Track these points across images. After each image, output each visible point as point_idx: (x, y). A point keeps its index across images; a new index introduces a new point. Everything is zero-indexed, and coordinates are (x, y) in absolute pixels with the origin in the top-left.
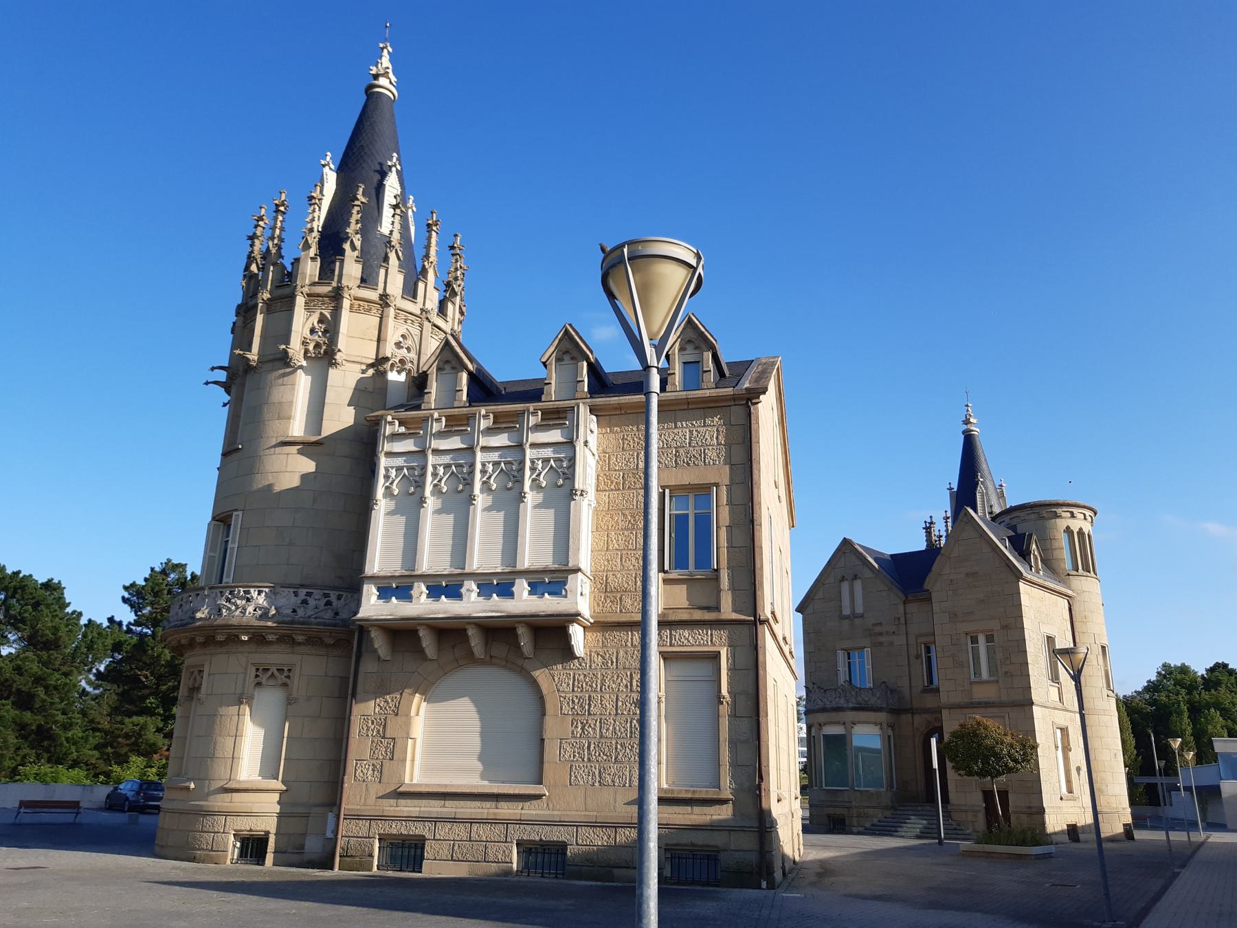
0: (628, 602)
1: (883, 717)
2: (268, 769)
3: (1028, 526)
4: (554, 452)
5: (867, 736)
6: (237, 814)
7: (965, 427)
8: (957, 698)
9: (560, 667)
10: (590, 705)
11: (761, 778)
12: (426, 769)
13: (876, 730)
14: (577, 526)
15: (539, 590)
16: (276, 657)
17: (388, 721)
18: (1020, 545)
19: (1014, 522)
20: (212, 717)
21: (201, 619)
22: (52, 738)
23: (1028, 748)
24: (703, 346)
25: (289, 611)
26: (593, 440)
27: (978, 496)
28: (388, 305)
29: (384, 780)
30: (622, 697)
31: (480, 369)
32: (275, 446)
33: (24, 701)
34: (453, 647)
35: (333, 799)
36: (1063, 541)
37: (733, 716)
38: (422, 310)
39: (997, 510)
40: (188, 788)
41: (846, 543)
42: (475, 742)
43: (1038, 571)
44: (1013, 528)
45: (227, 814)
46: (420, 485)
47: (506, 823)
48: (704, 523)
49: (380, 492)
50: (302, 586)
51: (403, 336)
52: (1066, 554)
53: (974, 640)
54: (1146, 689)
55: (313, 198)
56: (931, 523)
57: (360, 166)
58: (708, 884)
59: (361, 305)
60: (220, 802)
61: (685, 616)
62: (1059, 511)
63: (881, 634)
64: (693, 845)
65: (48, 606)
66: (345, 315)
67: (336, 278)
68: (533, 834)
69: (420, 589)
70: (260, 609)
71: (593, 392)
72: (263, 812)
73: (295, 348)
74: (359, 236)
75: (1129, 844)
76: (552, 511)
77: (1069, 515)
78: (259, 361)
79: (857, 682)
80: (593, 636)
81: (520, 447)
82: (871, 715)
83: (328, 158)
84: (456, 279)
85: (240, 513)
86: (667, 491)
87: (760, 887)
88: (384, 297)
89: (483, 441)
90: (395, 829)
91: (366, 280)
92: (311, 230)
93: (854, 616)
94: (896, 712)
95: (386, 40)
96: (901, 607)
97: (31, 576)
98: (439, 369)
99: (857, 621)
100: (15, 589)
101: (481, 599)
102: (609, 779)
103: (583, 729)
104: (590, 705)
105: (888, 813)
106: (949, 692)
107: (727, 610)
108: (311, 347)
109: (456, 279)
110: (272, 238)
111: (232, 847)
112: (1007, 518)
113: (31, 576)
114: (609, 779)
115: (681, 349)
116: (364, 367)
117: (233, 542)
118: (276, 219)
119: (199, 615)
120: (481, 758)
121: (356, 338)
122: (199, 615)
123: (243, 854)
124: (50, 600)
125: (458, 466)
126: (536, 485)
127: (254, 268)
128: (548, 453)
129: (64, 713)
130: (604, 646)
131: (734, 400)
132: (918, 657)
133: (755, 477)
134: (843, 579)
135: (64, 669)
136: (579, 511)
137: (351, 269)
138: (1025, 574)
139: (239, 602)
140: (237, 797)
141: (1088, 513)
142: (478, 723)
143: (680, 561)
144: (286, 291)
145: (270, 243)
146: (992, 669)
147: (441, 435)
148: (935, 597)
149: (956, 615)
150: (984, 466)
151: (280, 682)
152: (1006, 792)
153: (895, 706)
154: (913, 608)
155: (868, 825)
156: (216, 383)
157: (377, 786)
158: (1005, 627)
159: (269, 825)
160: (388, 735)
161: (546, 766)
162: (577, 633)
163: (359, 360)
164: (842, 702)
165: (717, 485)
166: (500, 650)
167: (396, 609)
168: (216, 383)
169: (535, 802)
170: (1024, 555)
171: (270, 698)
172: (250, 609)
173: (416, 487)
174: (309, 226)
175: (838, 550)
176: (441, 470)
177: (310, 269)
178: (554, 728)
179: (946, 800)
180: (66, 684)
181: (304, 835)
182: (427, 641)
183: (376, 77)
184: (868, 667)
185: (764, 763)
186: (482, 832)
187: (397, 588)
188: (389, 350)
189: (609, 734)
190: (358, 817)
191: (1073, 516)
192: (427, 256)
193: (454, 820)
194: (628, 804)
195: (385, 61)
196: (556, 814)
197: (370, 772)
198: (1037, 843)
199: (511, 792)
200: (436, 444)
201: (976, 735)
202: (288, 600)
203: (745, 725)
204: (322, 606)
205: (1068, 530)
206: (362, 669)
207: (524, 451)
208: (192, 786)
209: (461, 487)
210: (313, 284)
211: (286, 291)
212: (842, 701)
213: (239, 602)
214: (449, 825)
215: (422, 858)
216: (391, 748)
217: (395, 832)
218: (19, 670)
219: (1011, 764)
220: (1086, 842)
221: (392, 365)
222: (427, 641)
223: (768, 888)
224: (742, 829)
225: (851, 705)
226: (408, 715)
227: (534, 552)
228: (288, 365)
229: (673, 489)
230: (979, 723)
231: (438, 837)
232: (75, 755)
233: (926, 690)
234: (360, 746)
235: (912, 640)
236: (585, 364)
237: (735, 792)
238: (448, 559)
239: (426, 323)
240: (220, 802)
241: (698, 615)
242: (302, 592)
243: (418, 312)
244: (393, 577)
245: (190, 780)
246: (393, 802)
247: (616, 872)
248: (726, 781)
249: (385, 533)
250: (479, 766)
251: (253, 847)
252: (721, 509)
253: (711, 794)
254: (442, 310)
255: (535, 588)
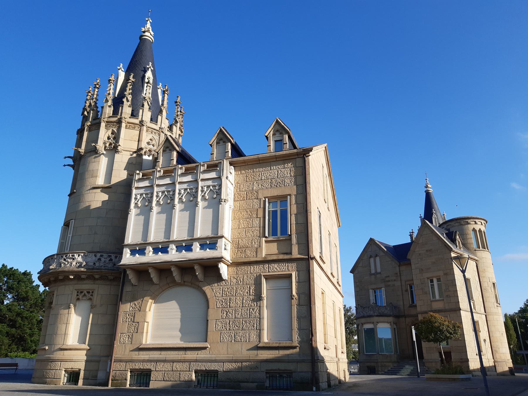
0: (248, 252)
1: (391, 319)
2: (82, 340)
3: (455, 228)
4: (213, 182)
5: (384, 331)
6: (66, 361)
7: (426, 189)
8: (424, 309)
9: (216, 285)
10: (230, 303)
11: (312, 335)
12: (154, 337)
13: (388, 326)
14: (227, 218)
15: (205, 247)
16: (86, 286)
17: (136, 314)
18: (451, 237)
19: (449, 227)
20: (57, 315)
21: (52, 269)
22: (25, 341)
23: (458, 327)
24: (284, 132)
25: (92, 264)
26: (232, 178)
27: (433, 219)
28: (143, 125)
29: (133, 342)
30: (245, 298)
31: (183, 151)
32: (90, 190)
33: (13, 324)
34: (167, 278)
35: (109, 354)
36: (472, 235)
37: (299, 305)
38: (160, 128)
39: (441, 222)
40: (45, 349)
41: (371, 241)
42: (177, 323)
43: (460, 248)
44: (448, 230)
45: (61, 361)
46: (150, 202)
47: (190, 361)
48: (284, 213)
49: (132, 205)
50: (98, 252)
51: (151, 140)
52: (473, 241)
53: (432, 281)
54: (520, 312)
55: (110, 80)
56: (412, 232)
57: (135, 68)
58: (287, 390)
59: (130, 125)
60: (59, 355)
61: (275, 257)
62: (469, 221)
63: (389, 281)
64: (279, 370)
65: (24, 282)
66: (123, 130)
67: (119, 114)
68: (203, 367)
69: (150, 249)
70: (79, 263)
71: (233, 156)
72: (78, 360)
73: (100, 145)
74: (130, 96)
75: (512, 377)
76: (212, 210)
77: (474, 223)
78: (85, 153)
79: (379, 304)
80: (233, 269)
81: (196, 181)
82: (386, 319)
83: (121, 66)
84: (178, 116)
85: (73, 221)
86: (267, 199)
87: (312, 390)
88: (141, 122)
89: (180, 179)
90: (138, 366)
91: (134, 115)
92: (109, 94)
93: (376, 273)
94: (397, 317)
95: (148, 17)
96: (398, 268)
97: (17, 269)
98: (164, 151)
99: (378, 276)
100: (10, 275)
101: (177, 253)
102: (239, 338)
103: (226, 314)
104: (230, 303)
105: (395, 365)
106: (421, 305)
107: (295, 253)
108: (107, 145)
109: (178, 116)
110: (93, 99)
111: (63, 378)
112: (445, 226)
113: (17, 269)
114: (239, 338)
115: (274, 135)
116: (132, 153)
117: (70, 234)
118: (94, 91)
119: (51, 267)
120: (181, 331)
121: (128, 140)
122: (51, 267)
123: (69, 381)
124: (25, 280)
125: (168, 192)
126: (204, 198)
127: (86, 113)
128: (210, 183)
129: (30, 329)
130: (237, 274)
131: (298, 155)
132: (407, 291)
133: (308, 190)
134: (371, 257)
135: (31, 310)
136: (223, 209)
137: (127, 110)
138: (453, 249)
139: (69, 260)
140: (66, 352)
141: (483, 222)
142: (179, 314)
143: (274, 232)
144: (97, 121)
145: (92, 101)
146: (441, 295)
147: (161, 178)
148: (413, 262)
149: (422, 270)
150: (435, 206)
151: (88, 298)
152: (450, 352)
153: (398, 316)
154: (403, 268)
155: (386, 370)
156: (69, 165)
157: (130, 345)
158: (446, 274)
159: (81, 366)
160: (135, 321)
161: (209, 333)
162: (224, 269)
163: (129, 150)
164: (372, 313)
165: (290, 195)
166: (188, 278)
167: (139, 259)
168: (69, 165)
169: (203, 351)
170: (453, 241)
171: (85, 305)
172: (74, 263)
173: (148, 203)
174: (108, 92)
175: (368, 243)
176: (160, 194)
177: (109, 111)
178: (213, 314)
179: (421, 357)
180: (30, 316)
181: (97, 370)
182: (153, 275)
183: (144, 32)
184: (384, 297)
185: (313, 328)
186: (178, 366)
187: (139, 249)
188: (143, 145)
189: (239, 316)
190: (121, 361)
191: (476, 223)
192: (163, 105)
193: (165, 361)
194: (248, 350)
195: (148, 25)
196: (213, 357)
197: (127, 339)
198: (463, 373)
199: (192, 346)
200: (158, 182)
201: (430, 322)
202: (92, 259)
203: (304, 309)
204: (108, 261)
205: (474, 230)
206: (124, 290)
207: (198, 183)
208: (47, 348)
209: (169, 201)
210: (110, 117)
211: (97, 121)
212: (372, 312)
213: (69, 260)
214: (163, 364)
215: (150, 380)
216: (137, 327)
217: (137, 367)
218: (10, 310)
219: (448, 335)
220: (490, 376)
221: (145, 152)
222: (153, 275)
223: (316, 391)
224: (303, 361)
225: (376, 314)
226: (145, 311)
227: (202, 230)
228: (97, 153)
229: (270, 198)
230: (431, 316)
231: (157, 369)
232: (34, 348)
233: (410, 306)
234: (123, 326)
235: (403, 283)
236: (229, 144)
237: (300, 343)
238: (163, 235)
239: (162, 134)
240: (59, 355)
241: (281, 257)
242: (99, 255)
243: (158, 129)
244: (137, 245)
245: (46, 345)
246: (137, 353)
247: (242, 385)
248: (296, 337)
249: (134, 225)
250: (179, 334)
251: (73, 376)
252: (292, 206)
253: (288, 344)
254: (170, 128)
255: (203, 247)
